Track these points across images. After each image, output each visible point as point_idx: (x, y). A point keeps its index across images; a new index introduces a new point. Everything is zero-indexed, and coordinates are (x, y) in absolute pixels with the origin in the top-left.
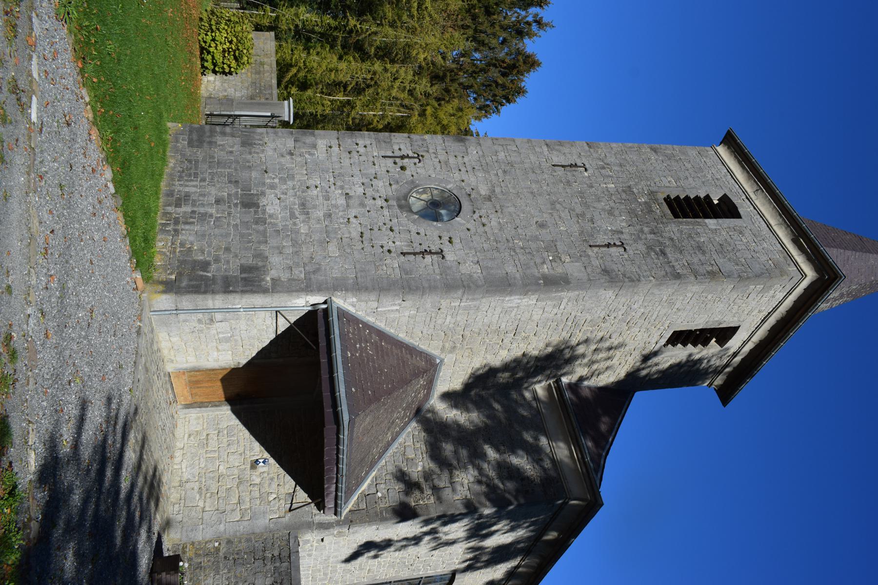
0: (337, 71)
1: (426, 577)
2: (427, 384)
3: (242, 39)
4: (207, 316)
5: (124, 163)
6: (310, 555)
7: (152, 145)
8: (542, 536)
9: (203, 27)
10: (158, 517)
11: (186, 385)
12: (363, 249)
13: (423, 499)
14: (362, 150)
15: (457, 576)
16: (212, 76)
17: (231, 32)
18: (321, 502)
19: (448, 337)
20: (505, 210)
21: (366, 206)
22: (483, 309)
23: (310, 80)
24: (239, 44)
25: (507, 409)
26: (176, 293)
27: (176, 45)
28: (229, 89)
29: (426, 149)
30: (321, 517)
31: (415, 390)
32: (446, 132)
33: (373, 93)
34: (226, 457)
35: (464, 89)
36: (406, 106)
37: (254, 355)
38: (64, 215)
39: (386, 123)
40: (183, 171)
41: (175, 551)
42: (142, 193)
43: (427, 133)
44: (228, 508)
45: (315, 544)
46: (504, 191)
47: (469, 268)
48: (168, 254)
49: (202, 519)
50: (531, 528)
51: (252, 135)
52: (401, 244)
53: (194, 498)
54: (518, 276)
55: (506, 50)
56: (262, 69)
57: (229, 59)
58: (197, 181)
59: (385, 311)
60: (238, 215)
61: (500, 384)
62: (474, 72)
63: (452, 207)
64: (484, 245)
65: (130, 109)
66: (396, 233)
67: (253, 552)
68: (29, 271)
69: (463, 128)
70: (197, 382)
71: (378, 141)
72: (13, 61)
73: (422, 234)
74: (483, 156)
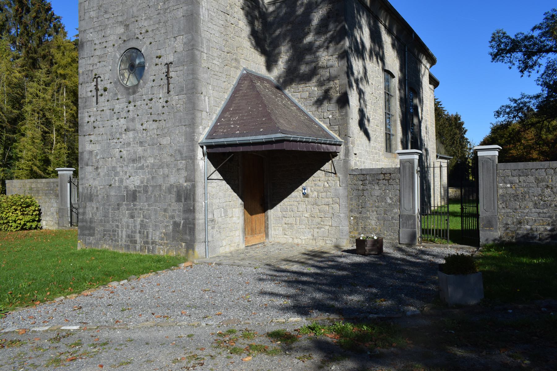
0: (33, 138)
1: (385, 89)
2: (260, 81)
3: (13, 202)
4: (210, 223)
5: (107, 275)
6: (364, 162)
7: (94, 258)
8: (367, 6)
9: (6, 228)
10: (333, 252)
11: (254, 237)
12: (165, 120)
13: (336, 88)
14: (92, 119)
15: (387, 68)
16: (42, 222)
17: (8, 210)
18: (332, 155)
19: (228, 63)
20: (135, 14)
21: (134, 117)
22: (209, 36)
23: (42, 157)
24: (17, 204)
25: (280, 25)
26: (194, 242)
27: (20, 245)
28: (52, 211)
29: (90, 72)
30: (341, 155)
31: (263, 89)
32: (77, 60)
33: (49, 112)
34: (299, 213)
35: (42, 44)
36: (58, 89)
37: (236, 195)
38: (142, 308)
39: (72, 104)
40: (112, 239)
41: (354, 242)
42: (127, 264)
43: (78, 73)
44: (331, 211)
45: (357, 159)
46: (121, 14)
47: (179, 44)
48: (168, 248)
49: (336, 227)
50: (361, 14)
51: (84, 195)
52: (162, 93)
53: (324, 231)
54: (185, 8)
55: (7, 7)
56: (35, 189)
57: (29, 211)
58: (118, 230)
59: (209, 107)
60: (141, 204)
61: (263, 28)
62: (28, 35)
63: (134, 54)
64: (162, 32)
65: (69, 272)
66: (154, 96)
67: (359, 197)
68: (178, 326)
69: (74, 47)
70: (252, 230)
71: (85, 107)
72: (37, 341)
73: (154, 77)
74: (94, 28)
